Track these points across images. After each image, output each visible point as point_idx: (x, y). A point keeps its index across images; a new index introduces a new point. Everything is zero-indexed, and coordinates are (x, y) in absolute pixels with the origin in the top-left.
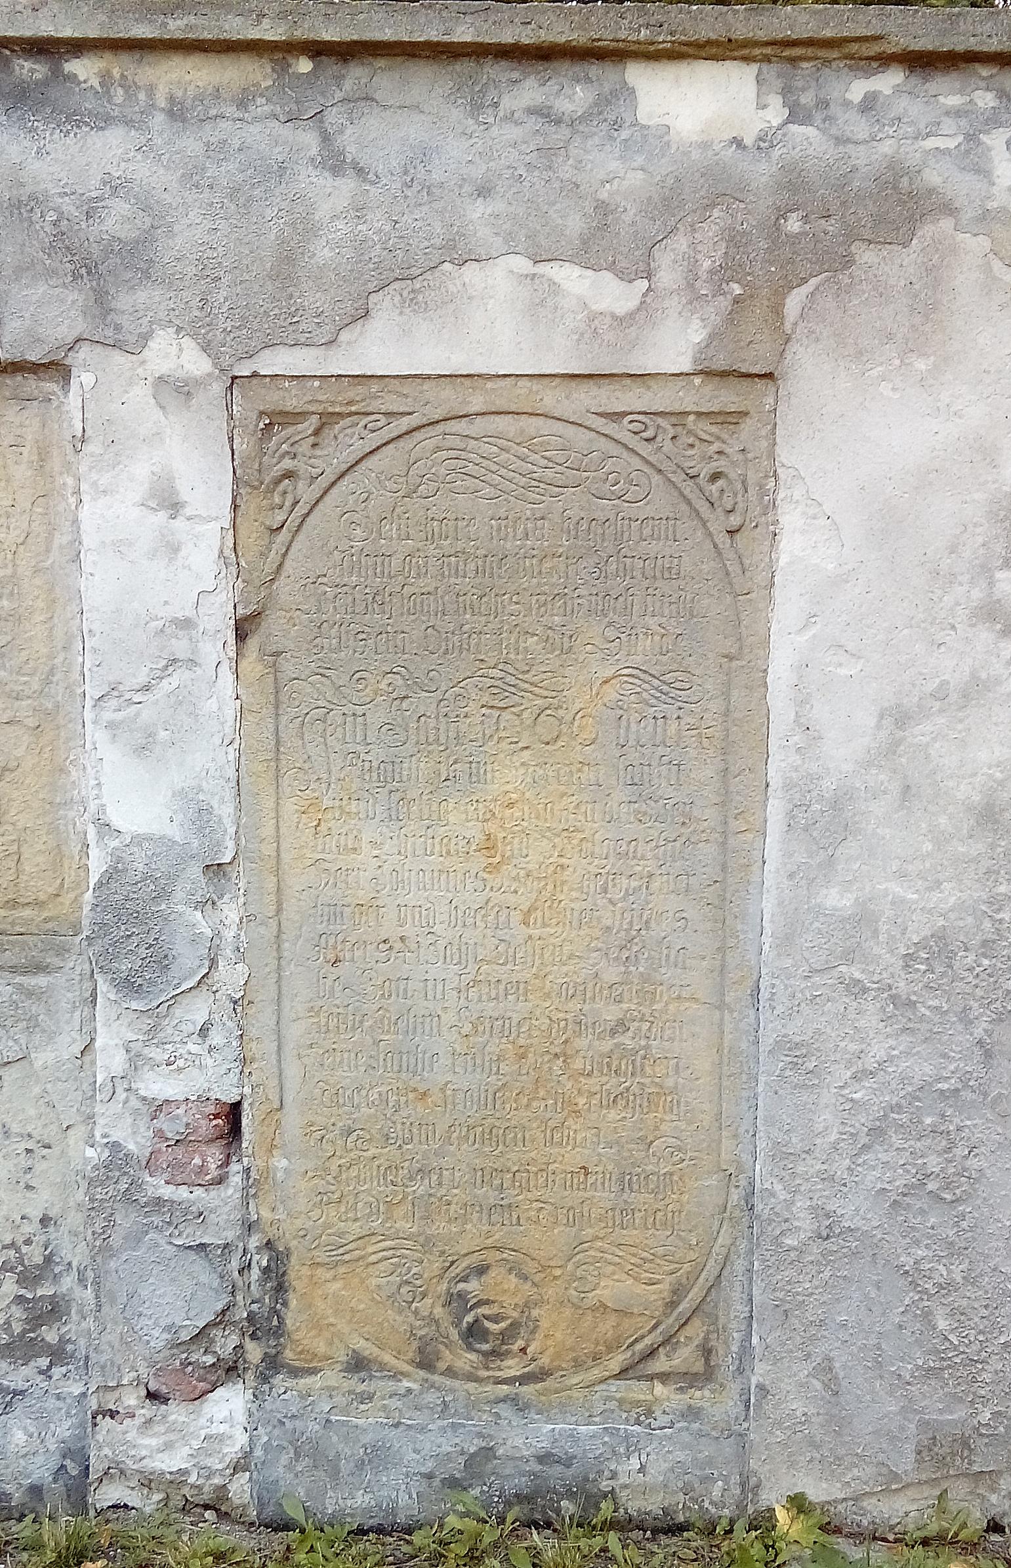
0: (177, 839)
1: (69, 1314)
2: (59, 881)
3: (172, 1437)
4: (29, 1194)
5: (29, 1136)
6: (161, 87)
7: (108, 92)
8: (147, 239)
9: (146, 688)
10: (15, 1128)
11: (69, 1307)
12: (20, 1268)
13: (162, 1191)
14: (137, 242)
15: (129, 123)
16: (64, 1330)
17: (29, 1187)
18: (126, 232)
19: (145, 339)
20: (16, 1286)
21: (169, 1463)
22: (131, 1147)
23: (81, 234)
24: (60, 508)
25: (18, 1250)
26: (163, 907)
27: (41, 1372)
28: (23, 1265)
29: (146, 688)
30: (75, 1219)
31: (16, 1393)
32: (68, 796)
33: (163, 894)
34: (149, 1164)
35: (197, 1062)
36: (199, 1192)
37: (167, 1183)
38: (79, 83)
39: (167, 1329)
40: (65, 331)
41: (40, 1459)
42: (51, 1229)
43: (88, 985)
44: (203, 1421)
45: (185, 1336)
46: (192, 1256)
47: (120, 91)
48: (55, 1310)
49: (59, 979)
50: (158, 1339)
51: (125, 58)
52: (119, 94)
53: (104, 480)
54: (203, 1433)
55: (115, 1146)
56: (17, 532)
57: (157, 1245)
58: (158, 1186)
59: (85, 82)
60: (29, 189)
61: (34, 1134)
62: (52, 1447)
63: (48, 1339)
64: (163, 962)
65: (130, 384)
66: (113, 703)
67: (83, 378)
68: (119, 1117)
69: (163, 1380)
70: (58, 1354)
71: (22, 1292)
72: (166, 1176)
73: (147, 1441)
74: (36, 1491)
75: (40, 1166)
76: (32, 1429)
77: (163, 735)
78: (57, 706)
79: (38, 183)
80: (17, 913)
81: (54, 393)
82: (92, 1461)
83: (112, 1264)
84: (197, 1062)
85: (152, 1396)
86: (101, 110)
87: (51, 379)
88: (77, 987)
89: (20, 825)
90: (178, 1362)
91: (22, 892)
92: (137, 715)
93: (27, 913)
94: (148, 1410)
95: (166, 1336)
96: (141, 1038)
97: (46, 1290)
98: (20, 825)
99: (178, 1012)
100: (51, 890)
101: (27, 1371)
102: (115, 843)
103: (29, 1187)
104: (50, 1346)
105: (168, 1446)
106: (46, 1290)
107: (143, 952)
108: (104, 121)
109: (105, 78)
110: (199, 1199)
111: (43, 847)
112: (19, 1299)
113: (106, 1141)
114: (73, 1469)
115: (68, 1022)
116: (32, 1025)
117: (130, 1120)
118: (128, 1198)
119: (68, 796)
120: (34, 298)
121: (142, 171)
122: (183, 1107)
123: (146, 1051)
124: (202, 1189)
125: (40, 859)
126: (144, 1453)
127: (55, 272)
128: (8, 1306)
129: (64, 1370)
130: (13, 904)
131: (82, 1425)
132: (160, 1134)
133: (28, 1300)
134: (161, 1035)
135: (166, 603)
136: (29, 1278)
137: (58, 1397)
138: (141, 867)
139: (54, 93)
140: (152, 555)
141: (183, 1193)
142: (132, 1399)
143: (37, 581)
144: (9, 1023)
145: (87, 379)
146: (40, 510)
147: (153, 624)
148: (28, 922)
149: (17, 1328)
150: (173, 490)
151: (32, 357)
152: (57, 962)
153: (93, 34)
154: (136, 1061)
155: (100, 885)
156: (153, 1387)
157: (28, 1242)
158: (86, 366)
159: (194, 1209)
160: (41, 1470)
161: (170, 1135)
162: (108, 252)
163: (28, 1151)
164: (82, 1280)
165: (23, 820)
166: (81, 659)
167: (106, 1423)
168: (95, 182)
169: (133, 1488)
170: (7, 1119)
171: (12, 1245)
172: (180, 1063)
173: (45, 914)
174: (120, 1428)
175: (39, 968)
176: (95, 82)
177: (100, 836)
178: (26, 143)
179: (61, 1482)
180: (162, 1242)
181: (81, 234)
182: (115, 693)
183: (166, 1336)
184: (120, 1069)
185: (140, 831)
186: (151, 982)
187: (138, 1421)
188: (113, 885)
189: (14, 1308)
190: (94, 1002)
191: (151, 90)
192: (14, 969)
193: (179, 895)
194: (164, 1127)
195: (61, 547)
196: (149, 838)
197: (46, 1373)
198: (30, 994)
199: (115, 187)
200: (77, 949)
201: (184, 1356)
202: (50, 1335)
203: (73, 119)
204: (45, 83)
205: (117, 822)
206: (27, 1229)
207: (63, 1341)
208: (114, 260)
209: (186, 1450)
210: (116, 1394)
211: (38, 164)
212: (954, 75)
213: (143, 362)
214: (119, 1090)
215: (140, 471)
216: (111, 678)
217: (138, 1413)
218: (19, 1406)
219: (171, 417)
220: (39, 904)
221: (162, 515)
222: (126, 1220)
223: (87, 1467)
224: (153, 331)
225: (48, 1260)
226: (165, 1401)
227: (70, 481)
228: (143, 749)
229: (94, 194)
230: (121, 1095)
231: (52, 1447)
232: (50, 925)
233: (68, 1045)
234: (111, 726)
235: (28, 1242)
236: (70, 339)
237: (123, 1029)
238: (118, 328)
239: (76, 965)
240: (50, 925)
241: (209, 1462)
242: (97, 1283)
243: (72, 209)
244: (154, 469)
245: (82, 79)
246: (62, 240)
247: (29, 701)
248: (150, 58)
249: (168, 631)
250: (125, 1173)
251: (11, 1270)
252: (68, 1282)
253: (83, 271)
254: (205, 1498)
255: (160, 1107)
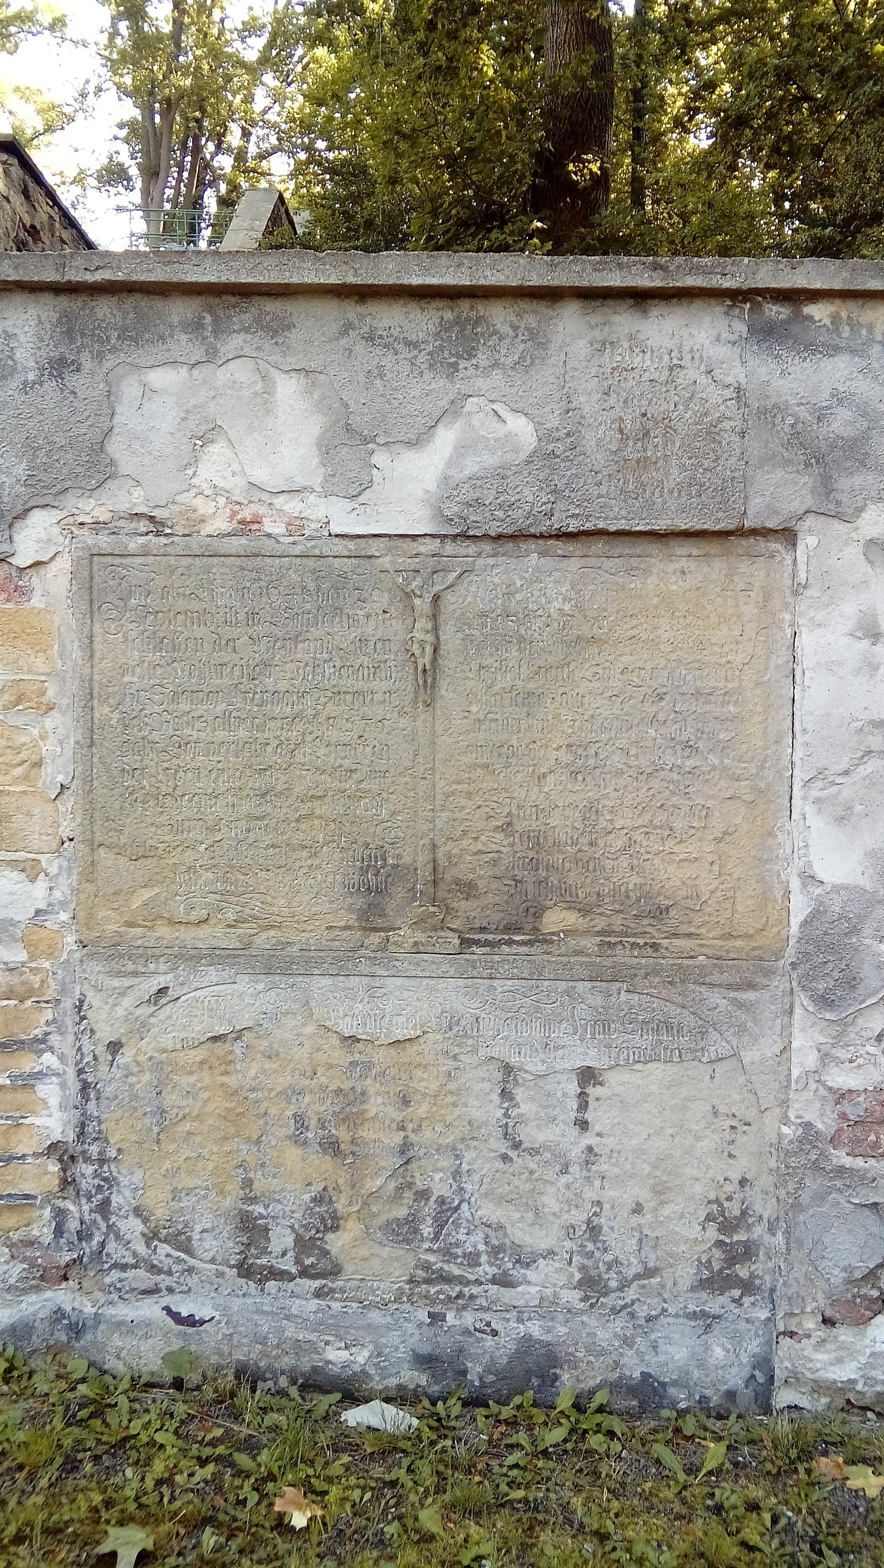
0: (868, 888)
1: (757, 1255)
2: (764, 919)
3: (843, 1353)
4: (731, 1161)
5: (734, 1115)
6: (878, 326)
7: (837, 329)
8: (865, 437)
9: (846, 773)
10: (722, 1109)
11: (758, 1249)
12: (721, 1219)
13: (843, 1160)
14: (856, 440)
15: (853, 352)
16: (753, 1267)
17: (730, 1156)
18: (849, 432)
19: (860, 510)
20: (716, 1233)
21: (843, 1373)
22: (820, 1126)
23: (813, 434)
24: (778, 637)
25: (720, 1205)
26: (854, 940)
27: (734, 1301)
28: (723, 1216)
29: (846, 773)
30: (766, 1181)
31: (715, 1317)
32: (775, 854)
33: (854, 930)
34: (834, 1141)
35: (873, 1061)
36: (872, 1162)
37: (847, 1154)
38: (815, 322)
39: (844, 1269)
40: (797, 506)
41: (734, 1370)
42: (747, 1189)
43: (787, 999)
44: (867, 1341)
45: (858, 1275)
46: (867, 1212)
47: (847, 328)
48: (748, 1252)
49: (766, 995)
50: (837, 1276)
51: (851, 304)
52: (846, 331)
53: (820, 616)
54: (868, 1351)
55: (808, 1125)
56: (744, 655)
57: (839, 1203)
58: (841, 1157)
59: (820, 321)
60: (773, 400)
61: (737, 1114)
62: (745, 1361)
63: (741, 1275)
64: (851, 983)
65: (846, 545)
66: (820, 784)
67: (807, 541)
68: (810, 1102)
69: (836, 1308)
70: (748, 1287)
71: (722, 1237)
72: (847, 1149)
73: (819, 1356)
74: (731, 1395)
75: (741, 1139)
76: (729, 1346)
77: (858, 808)
78: (769, 786)
79: (780, 396)
80: (731, 943)
81: (778, 551)
82: (777, 1372)
83: (802, 1218)
84: (873, 1061)
85: (825, 1321)
86: (831, 342)
87: (776, 541)
88: (779, 1001)
89: (735, 876)
90: (850, 1296)
91: (737, 927)
92: (839, 793)
93: (739, 943)
94: (823, 1332)
95: (844, 1274)
96: (830, 1041)
97: (741, 1236)
98: (735, 876)
99: (860, 1022)
100: (759, 926)
101: (724, 1299)
102: (818, 891)
103: (730, 1156)
104: (741, 1280)
105: (839, 1361)
106: (741, 1236)
107: (836, 975)
108: (834, 350)
109: (835, 319)
110: (872, 1166)
111: (753, 893)
112: (719, 1244)
113: (799, 1121)
114: (760, 1378)
115: (770, 1028)
116: (742, 1030)
117: (818, 1105)
118: (816, 1167)
119: (775, 854)
120: (774, 481)
121: (863, 387)
122: (863, 1095)
123: (834, 1051)
124: (873, 1160)
125: (750, 902)
126: (818, 1365)
127: (791, 462)
128: (710, 1249)
129: (752, 1299)
130: (729, 936)
131: (769, 1343)
132: (843, 1116)
133: (726, 1244)
134: (846, 1039)
135: (866, 708)
136: (727, 1226)
137: (748, 1321)
138: (837, 909)
139: (795, 329)
140: (857, 672)
141: (860, 1162)
142: (810, 1324)
143: (757, 692)
144: (724, 1028)
145: (812, 541)
146: (762, 638)
147: (854, 725)
148: (739, 950)
149: (716, 1266)
150: (876, 624)
151: (770, 525)
152: (765, 981)
153: (836, 287)
154: (825, 1058)
155: (805, 924)
156: (828, 1313)
157: (729, 1199)
158: (810, 531)
159: (868, 1175)
160: (735, 1378)
161: (852, 1117)
162: (833, 447)
163: (732, 1127)
164: (772, 1231)
165: (738, 872)
166: (790, 750)
167: (786, 1341)
168: (826, 395)
169: (804, 1393)
170: (716, 1102)
171: (717, 1201)
172: (861, 1061)
173: (753, 944)
174: (798, 1346)
175: (751, 986)
176: (827, 321)
177: (804, 885)
178: (773, 366)
179: (751, 1388)
180: (842, 1201)
181: (813, 434)
182: (821, 776)
183: (844, 1274)
184: (813, 1065)
185: (839, 882)
186: (840, 998)
187: (813, 1341)
188: (815, 923)
189: (714, 1249)
190: (791, 1012)
191: (871, 328)
192: (730, 987)
193: (867, 931)
194: (848, 1111)
195: (777, 666)
196: (846, 887)
197: (737, 1302)
198: (740, 1005)
199: (840, 398)
200: (780, 972)
201: (856, 1290)
202: (743, 1272)
203: (810, 348)
204: (788, 321)
205: (821, 875)
206: (729, 1188)
207: (752, 1276)
208: (837, 453)
209: (854, 1365)
210: (797, 1319)
211: (781, 382)
212: (187, 299)
213: (857, 529)
214: (811, 1081)
215: (850, 609)
216: (819, 765)
217: (813, 1334)
218: (717, 1329)
219: (878, 570)
220: (748, 936)
221: (865, 643)
222: (813, 1184)
223: (772, 1377)
224: (866, 505)
225: (744, 1213)
226: (833, 1324)
227: (788, 617)
228: (843, 817)
229: (824, 404)
230: (813, 1086)
231: (745, 1361)
232: (756, 953)
233: (769, 1047)
234: (817, 801)
235: (729, 1199)
236: (801, 512)
237: (816, 1034)
238: (839, 503)
239: (779, 984)
240: (756, 953)
241: (873, 1373)
242: (787, 1233)
243: (807, 415)
244: (861, 608)
245: (817, 319)
246: (798, 437)
247: (748, 782)
248: (870, 304)
249: (866, 729)
250: (815, 1147)
251: (714, 1220)
252: (759, 1231)
253: (813, 461)
254: (866, 1402)
255: (842, 1096)
